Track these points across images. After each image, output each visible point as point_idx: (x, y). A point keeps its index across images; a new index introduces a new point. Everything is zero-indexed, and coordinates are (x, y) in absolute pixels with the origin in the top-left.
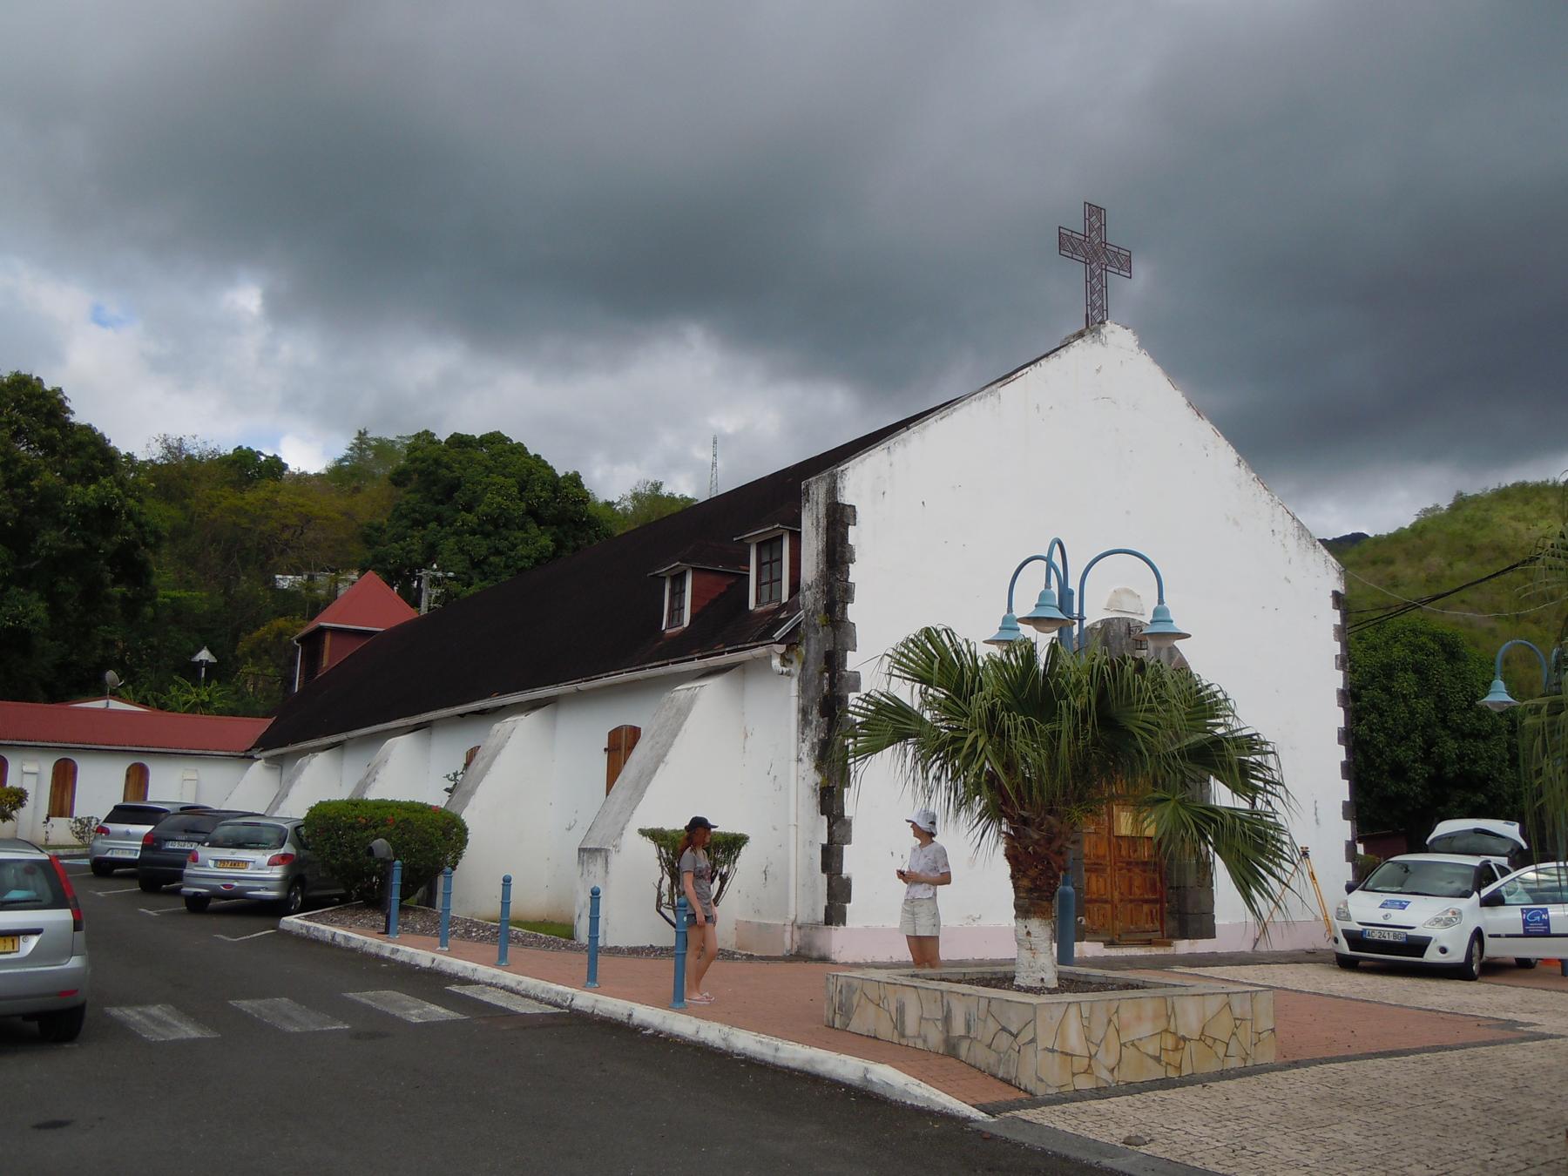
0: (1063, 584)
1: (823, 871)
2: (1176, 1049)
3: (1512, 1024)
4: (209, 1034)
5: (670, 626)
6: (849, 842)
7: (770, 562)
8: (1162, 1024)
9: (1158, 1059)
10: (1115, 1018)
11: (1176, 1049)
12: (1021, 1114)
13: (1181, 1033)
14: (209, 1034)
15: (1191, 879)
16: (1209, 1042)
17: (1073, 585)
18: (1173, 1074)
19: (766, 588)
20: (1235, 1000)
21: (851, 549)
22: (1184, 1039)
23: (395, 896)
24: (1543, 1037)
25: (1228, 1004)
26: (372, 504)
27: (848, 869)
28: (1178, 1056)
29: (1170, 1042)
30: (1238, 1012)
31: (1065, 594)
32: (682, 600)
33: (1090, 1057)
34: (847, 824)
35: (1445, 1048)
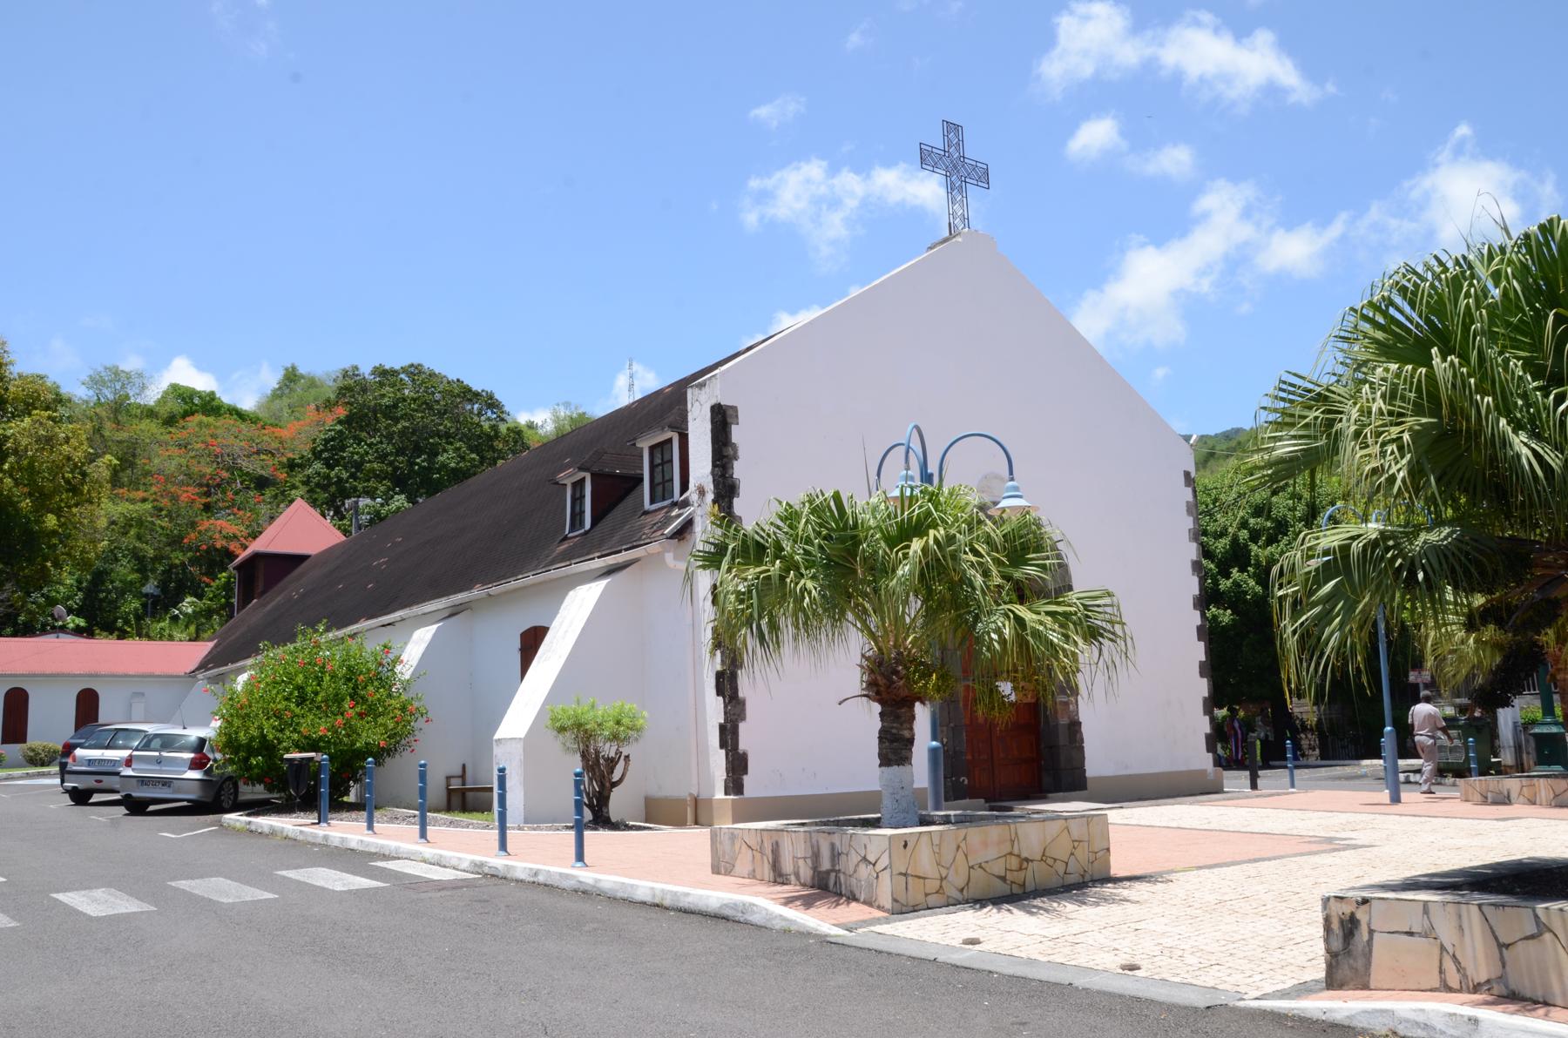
0: (924, 465)
1: (722, 747)
2: (1021, 869)
3: (1330, 840)
4: (146, 907)
5: (572, 529)
6: (744, 719)
7: (663, 464)
8: (1006, 848)
9: (1003, 879)
10: (963, 845)
11: (1021, 869)
12: (878, 928)
13: (1024, 855)
14: (146, 907)
15: (1063, 740)
16: (1050, 861)
17: (933, 468)
18: (1016, 890)
19: (660, 488)
20: (1073, 824)
21: (735, 447)
22: (1027, 860)
23: (324, 790)
24: (1355, 847)
25: (1067, 828)
26: (303, 432)
27: (743, 746)
28: (1022, 874)
29: (1014, 863)
30: (1075, 835)
31: (927, 478)
32: (583, 497)
33: (942, 879)
34: (742, 703)
35: (1263, 860)
